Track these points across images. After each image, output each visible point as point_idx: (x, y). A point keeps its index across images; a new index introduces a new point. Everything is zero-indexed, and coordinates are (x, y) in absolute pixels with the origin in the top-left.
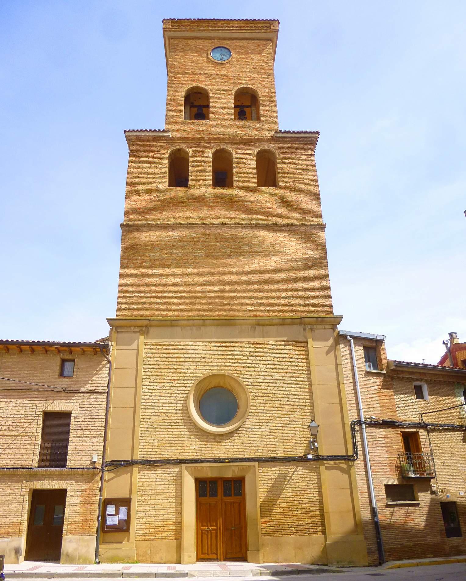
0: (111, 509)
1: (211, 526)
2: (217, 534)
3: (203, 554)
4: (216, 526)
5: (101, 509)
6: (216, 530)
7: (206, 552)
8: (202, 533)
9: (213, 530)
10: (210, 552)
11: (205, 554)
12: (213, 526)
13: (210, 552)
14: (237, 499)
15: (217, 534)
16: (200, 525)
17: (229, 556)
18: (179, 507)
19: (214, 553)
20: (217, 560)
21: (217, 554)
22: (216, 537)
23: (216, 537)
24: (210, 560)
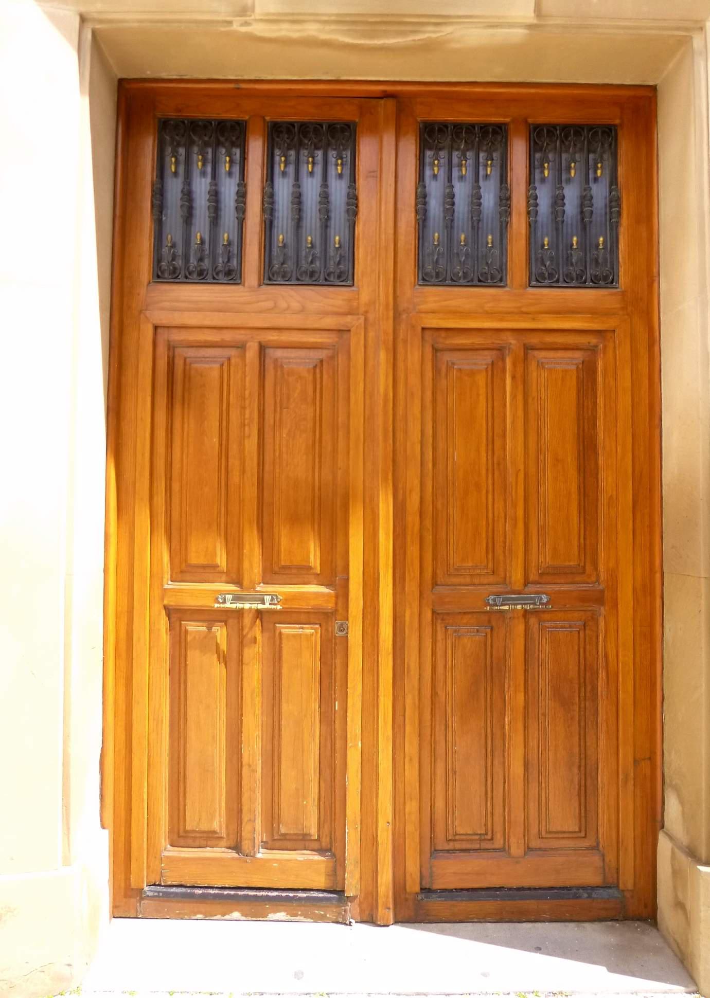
0: (196, 557)
1: (275, 571)
2: (333, 651)
3: (181, 836)
4: (334, 574)
5: (659, 679)
6: (329, 618)
7: (218, 823)
8: (180, 643)
9: (292, 614)
10: (256, 827)
11: (208, 838)
12: (300, 573)
13: (256, 827)
14: (572, 307)
15: (333, 651)
16: (154, 554)
17: (453, 872)
18: (645, 766)
19: (299, 841)
20: (329, 900)
21: (331, 847)
22: (331, 681)
23: (331, 681)
24: (254, 900)
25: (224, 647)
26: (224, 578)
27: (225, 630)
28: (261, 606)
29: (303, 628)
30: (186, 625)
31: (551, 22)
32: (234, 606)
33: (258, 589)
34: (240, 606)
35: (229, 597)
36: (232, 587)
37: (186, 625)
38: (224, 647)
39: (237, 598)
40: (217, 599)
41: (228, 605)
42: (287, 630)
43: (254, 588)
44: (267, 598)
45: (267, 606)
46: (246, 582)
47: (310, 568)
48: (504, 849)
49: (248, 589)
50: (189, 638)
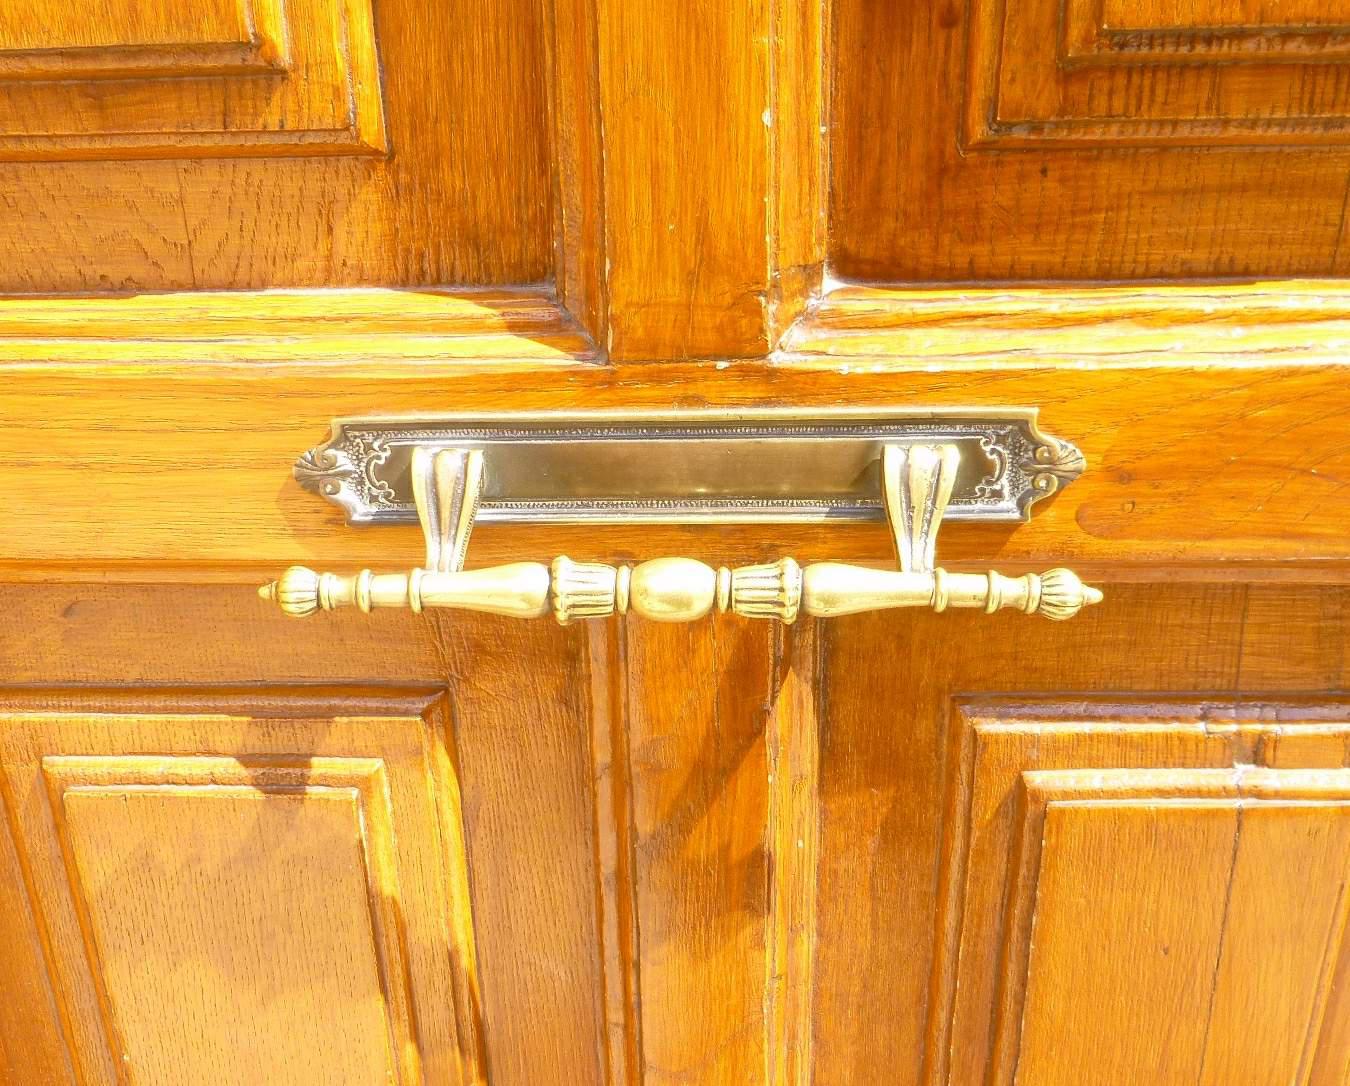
25: (445, 917)
26: (365, 217)
27: (440, 785)
28: (845, 587)
29: (1259, 753)
30: (38, 746)
31: (915, 35)
32: (514, 588)
33: (794, 347)
34: (584, 585)
35: (448, 466)
36: (471, 340)
37: (38, 746)
38: (445, 917)
39: (549, 471)
40: (311, 482)
41: (447, 579)
42: (1091, 773)
43: (743, 347)
44: (918, 468)
45: (915, 577)
46: (641, 288)
47: (251, 72)
48: (962, 166)
49: (669, 358)
50: (98, 869)
